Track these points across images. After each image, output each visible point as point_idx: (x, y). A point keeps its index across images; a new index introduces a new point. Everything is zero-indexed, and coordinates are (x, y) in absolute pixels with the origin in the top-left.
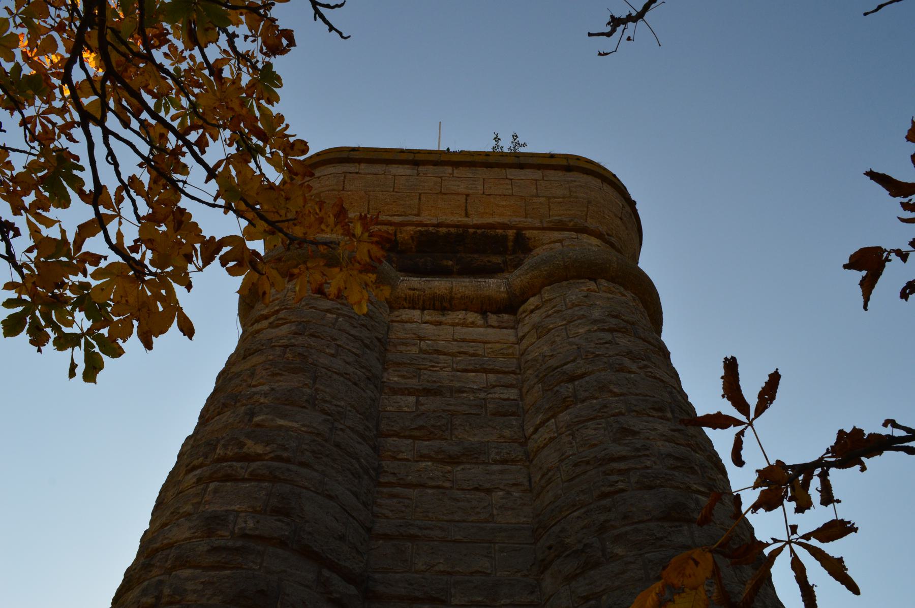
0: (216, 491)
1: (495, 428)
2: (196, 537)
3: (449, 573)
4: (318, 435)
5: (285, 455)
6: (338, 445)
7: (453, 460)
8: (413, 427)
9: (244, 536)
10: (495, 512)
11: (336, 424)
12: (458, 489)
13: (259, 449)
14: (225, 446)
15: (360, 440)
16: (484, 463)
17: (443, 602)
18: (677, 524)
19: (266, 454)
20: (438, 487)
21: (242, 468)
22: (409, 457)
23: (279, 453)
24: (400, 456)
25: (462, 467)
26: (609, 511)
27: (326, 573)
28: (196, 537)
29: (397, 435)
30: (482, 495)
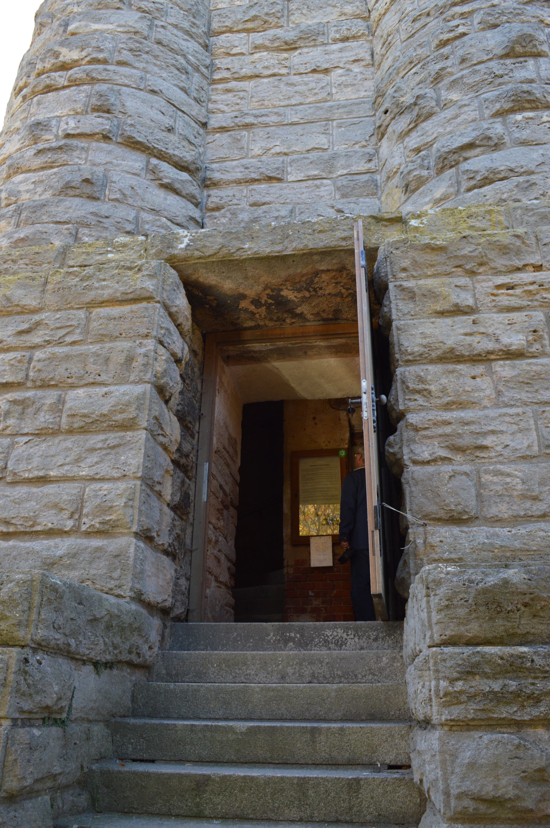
0: (39, 103)
1: (335, 6)
2: (25, 147)
3: (286, 154)
4: (136, 33)
5: (101, 56)
6: (159, 43)
7: (290, 47)
8: (246, 19)
9: (68, 136)
10: (334, 91)
11: (156, 22)
12: (295, 74)
13: (75, 55)
14: (43, 60)
15: (186, 37)
16: (323, 44)
17: (279, 180)
18: (522, 59)
19: (82, 59)
20: (274, 75)
21: (61, 77)
22: (244, 51)
23: (94, 55)
24: (234, 51)
25: (299, 51)
26: (446, 59)
27: (154, 161)
28: (25, 147)
29: (231, 31)
30: (321, 76)
